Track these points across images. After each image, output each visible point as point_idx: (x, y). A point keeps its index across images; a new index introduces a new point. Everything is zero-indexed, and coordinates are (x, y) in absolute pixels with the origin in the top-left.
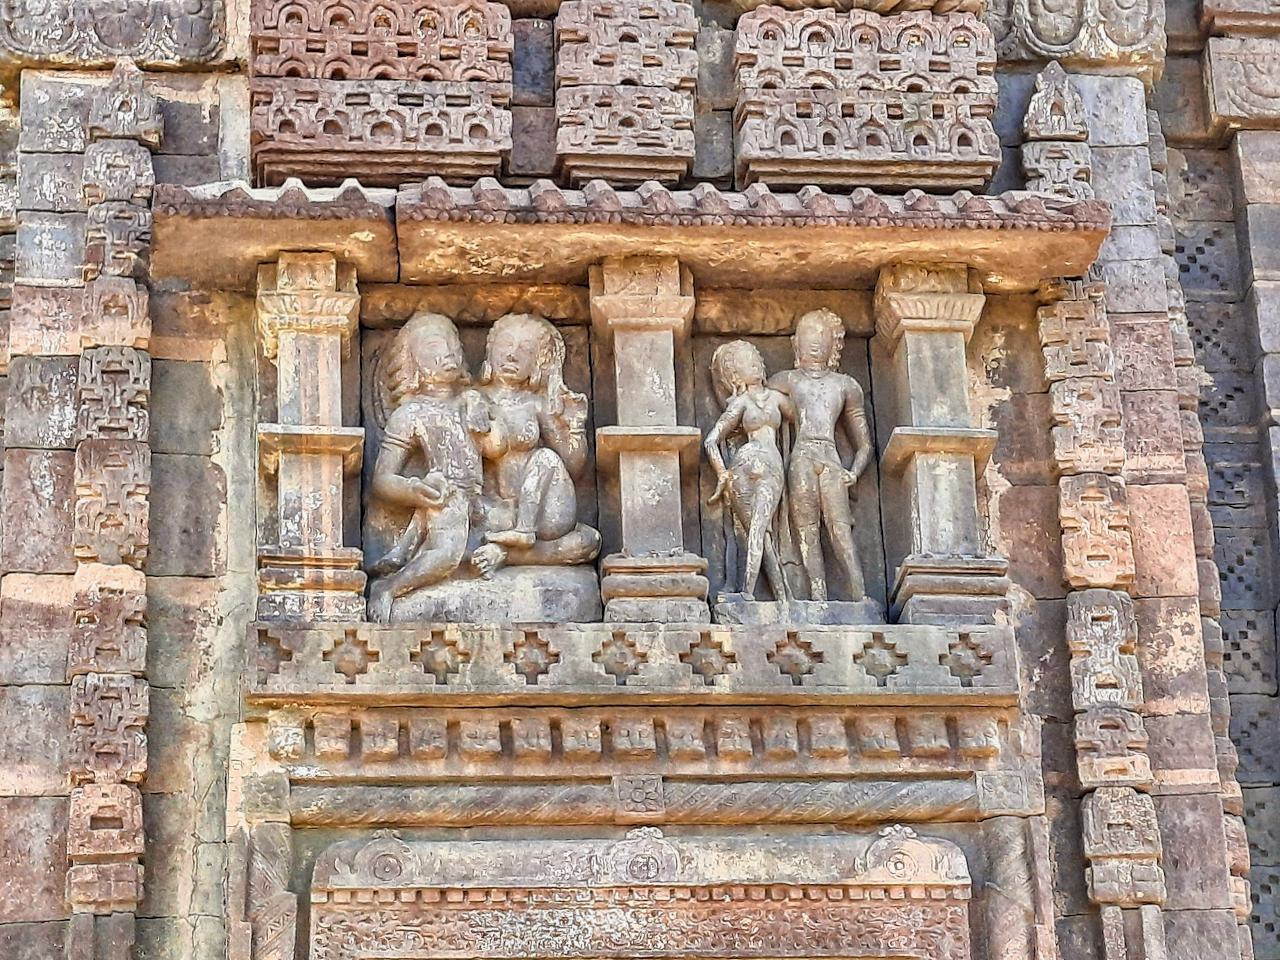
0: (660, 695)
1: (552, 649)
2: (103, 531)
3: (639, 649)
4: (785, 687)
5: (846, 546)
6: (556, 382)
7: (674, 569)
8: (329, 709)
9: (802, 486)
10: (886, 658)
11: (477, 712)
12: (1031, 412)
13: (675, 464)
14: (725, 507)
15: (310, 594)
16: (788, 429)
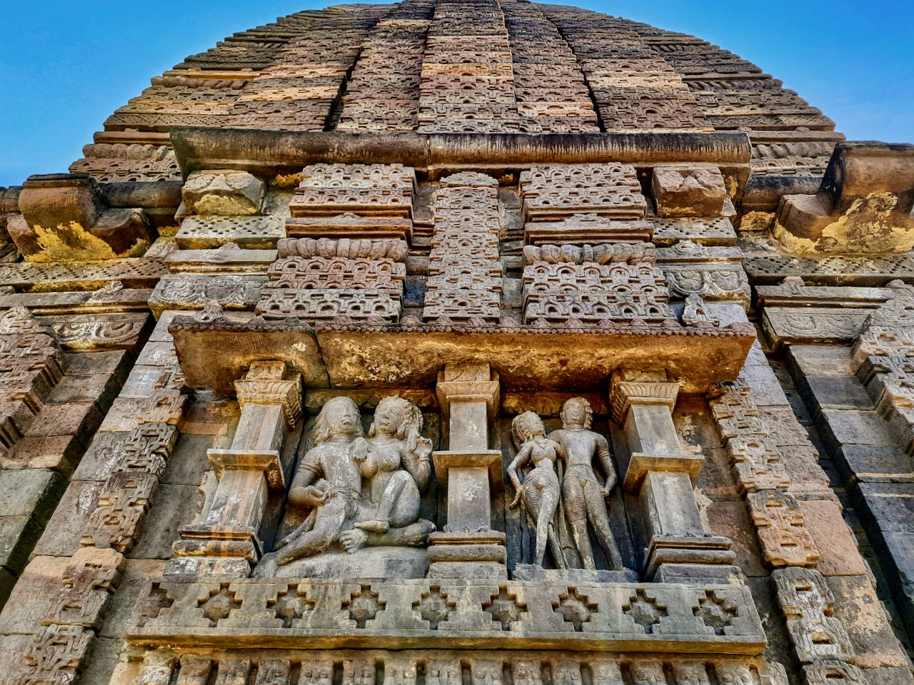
0: (462, 639)
1: (381, 599)
2: (105, 527)
3: (450, 600)
4: (569, 633)
5: (608, 534)
6: (414, 432)
7: (482, 541)
8: (195, 650)
9: (573, 493)
10: (648, 610)
11: (315, 654)
12: (716, 455)
13: (486, 475)
14: (521, 510)
15: (207, 560)
16: (560, 461)
